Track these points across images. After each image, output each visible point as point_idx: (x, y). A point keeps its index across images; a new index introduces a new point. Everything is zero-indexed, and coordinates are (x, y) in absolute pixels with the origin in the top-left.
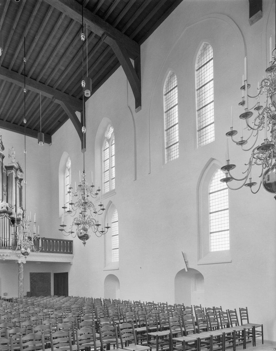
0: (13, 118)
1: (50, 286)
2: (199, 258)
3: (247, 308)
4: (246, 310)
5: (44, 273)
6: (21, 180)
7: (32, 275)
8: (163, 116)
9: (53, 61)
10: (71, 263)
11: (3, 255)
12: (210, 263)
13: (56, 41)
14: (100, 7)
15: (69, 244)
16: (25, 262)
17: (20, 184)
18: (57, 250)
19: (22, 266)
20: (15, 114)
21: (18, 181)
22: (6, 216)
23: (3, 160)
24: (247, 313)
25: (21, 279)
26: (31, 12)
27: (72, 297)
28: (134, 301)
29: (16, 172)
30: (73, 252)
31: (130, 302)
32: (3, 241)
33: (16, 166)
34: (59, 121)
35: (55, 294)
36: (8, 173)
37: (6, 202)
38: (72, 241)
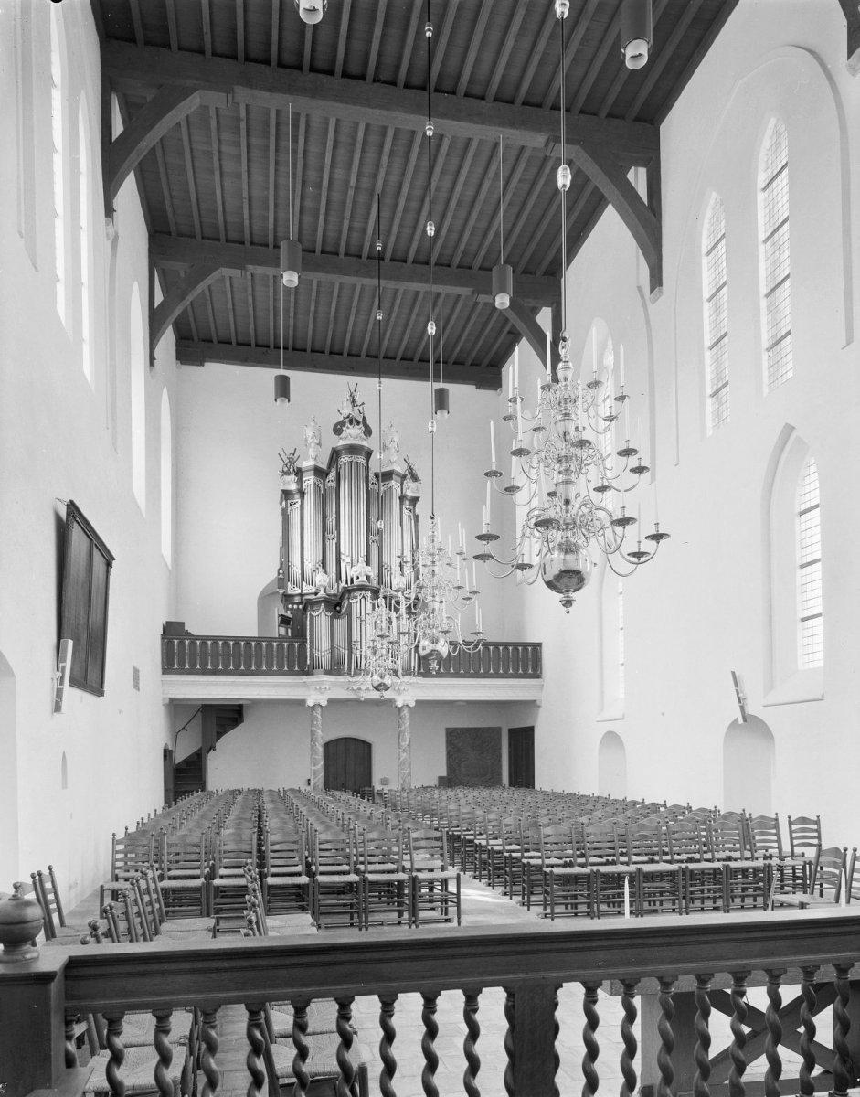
0: (398, 349)
1: (500, 761)
2: (770, 686)
3: (818, 817)
4: (817, 822)
5: (484, 728)
6: (414, 500)
7: (453, 735)
8: (701, 311)
9: (454, 217)
10: (538, 703)
11: (359, 689)
12: (791, 701)
13: (448, 179)
14: (528, 92)
15: (198, 648)
16: (412, 704)
17: (412, 510)
18: (506, 670)
19: (318, 714)
20: (402, 340)
21: (407, 502)
22: (363, 597)
23: (368, 461)
24: (818, 831)
25: (405, 744)
26: (381, 146)
27: (690, 808)
28: (789, 818)
29: (402, 484)
30: (543, 672)
31: (748, 816)
32: (359, 656)
33: (400, 468)
34: (509, 332)
35: (512, 784)
36: (382, 489)
37: (365, 564)
38: (540, 645)
